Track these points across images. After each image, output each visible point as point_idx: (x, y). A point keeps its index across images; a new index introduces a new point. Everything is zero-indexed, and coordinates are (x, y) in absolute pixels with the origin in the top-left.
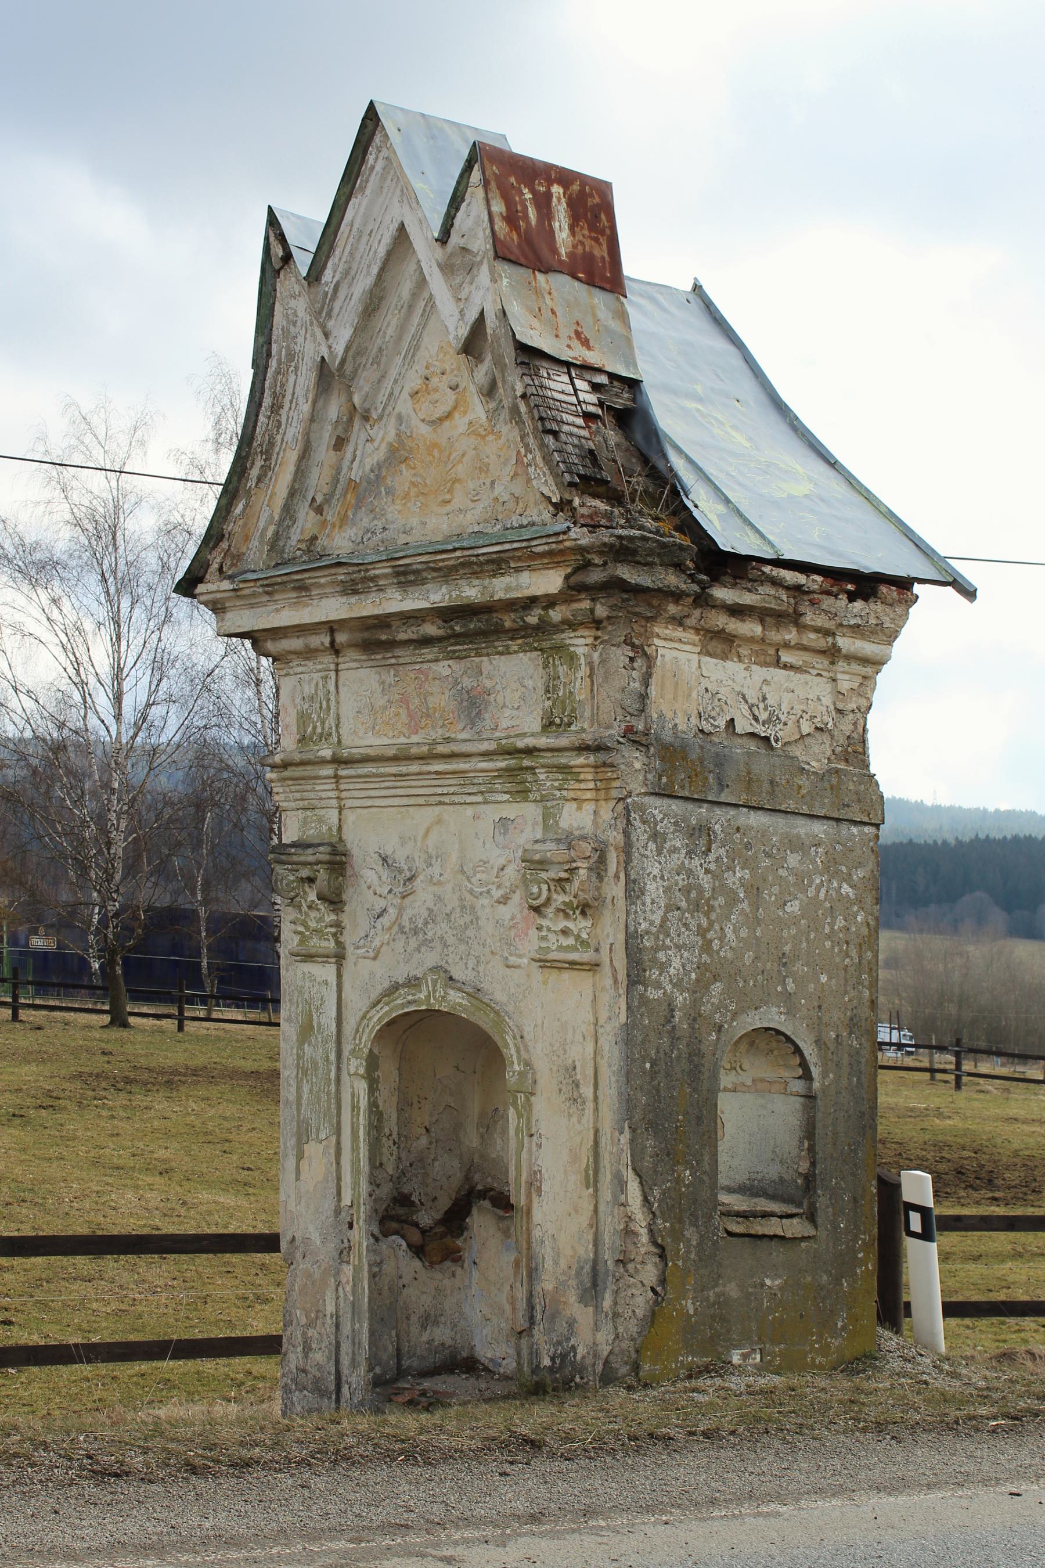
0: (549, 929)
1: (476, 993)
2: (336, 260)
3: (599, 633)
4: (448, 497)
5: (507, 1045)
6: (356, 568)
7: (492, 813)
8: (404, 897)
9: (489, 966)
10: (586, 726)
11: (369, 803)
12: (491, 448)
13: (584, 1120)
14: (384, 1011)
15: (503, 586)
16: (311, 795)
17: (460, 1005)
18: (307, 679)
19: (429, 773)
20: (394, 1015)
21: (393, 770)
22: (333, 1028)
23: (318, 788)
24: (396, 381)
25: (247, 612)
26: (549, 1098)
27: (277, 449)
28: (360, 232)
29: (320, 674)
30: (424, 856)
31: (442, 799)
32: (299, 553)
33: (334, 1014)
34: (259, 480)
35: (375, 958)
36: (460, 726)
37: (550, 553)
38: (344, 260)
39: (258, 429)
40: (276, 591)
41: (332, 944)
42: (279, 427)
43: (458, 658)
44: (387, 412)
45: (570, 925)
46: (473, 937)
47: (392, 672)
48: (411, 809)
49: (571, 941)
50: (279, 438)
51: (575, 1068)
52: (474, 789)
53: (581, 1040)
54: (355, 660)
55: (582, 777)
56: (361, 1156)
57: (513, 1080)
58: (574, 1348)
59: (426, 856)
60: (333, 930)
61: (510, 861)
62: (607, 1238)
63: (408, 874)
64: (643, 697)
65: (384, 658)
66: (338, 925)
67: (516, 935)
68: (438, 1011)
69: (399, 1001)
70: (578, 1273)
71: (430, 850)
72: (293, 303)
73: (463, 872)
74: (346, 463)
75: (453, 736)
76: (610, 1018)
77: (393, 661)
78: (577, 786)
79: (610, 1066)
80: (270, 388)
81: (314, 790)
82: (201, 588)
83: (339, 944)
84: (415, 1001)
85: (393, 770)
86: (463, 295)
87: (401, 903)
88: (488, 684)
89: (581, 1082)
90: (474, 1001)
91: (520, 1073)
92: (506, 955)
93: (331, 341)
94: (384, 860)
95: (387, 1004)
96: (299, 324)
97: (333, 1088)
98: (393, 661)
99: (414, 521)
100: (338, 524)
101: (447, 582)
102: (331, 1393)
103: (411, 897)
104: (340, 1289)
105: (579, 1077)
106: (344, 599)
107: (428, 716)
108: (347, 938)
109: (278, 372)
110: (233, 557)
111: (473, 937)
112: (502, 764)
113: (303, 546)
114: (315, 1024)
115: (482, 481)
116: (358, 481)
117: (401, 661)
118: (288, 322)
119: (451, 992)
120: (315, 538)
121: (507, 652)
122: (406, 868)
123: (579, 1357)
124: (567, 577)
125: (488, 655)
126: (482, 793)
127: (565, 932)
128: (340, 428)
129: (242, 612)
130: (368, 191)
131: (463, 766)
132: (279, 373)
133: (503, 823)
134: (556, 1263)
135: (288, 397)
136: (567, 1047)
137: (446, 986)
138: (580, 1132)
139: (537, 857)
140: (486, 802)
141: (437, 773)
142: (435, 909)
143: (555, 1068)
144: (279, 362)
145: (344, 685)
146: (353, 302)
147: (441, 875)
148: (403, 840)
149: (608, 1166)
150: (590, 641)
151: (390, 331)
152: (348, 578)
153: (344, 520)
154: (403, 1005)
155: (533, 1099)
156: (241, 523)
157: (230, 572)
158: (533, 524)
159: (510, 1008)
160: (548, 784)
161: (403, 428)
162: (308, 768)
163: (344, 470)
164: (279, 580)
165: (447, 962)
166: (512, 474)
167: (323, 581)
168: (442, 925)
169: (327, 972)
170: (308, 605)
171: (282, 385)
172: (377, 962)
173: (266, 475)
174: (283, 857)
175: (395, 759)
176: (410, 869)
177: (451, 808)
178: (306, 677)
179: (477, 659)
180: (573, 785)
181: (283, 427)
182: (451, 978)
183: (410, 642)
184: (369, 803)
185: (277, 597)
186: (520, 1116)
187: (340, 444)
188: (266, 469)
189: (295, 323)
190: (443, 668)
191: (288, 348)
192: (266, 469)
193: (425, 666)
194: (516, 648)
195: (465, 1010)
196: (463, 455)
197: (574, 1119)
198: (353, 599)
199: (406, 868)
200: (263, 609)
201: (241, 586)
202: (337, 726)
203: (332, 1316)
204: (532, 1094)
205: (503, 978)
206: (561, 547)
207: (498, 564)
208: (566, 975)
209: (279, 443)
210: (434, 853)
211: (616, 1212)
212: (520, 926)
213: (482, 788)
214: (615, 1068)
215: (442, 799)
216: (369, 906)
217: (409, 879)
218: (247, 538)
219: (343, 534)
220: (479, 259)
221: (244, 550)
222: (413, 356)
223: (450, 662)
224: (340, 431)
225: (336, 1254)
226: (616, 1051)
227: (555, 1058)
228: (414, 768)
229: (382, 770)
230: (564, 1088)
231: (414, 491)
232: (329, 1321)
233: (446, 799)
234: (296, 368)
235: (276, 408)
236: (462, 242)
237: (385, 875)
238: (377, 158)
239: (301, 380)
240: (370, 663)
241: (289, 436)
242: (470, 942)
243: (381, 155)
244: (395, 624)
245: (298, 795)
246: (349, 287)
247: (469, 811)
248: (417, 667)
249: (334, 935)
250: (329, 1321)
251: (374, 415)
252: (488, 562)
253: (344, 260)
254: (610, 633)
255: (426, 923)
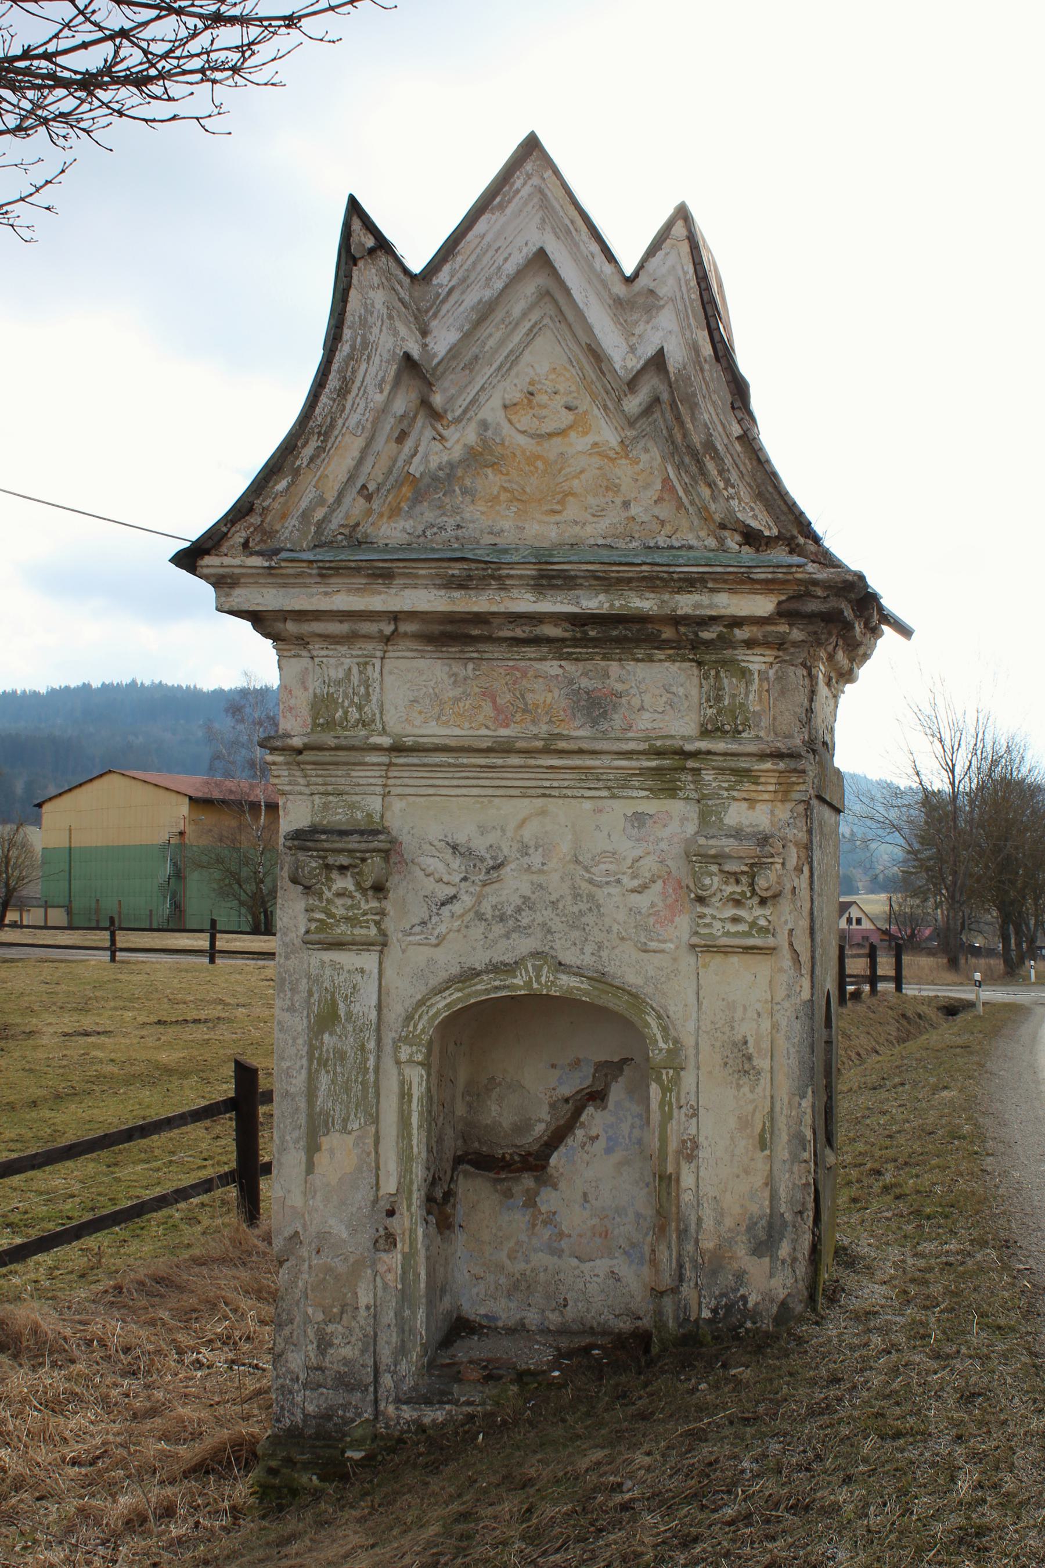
0: (714, 917)
1: (600, 979)
2: (457, 266)
3: (781, 653)
4: (558, 507)
5: (648, 1025)
6: (483, 566)
7: (619, 809)
9: (617, 951)
10: (762, 734)
12: (624, 472)
13: (759, 1090)
15: (690, 603)
16: (342, 781)
17: (578, 989)
18: (338, 664)
19: (539, 767)
21: (482, 761)
22: (373, 1015)
23: (354, 774)
24: (482, 388)
25: (273, 591)
26: (710, 1072)
27: (336, 433)
28: (489, 246)
29: (356, 660)
30: (516, 846)
31: (547, 792)
32: (340, 537)
33: (374, 1001)
34: (312, 460)
36: (577, 723)
37: (767, 581)
38: (465, 267)
39: (318, 410)
40: (330, 576)
41: (373, 931)
42: (343, 411)
43: (577, 660)
44: (468, 416)
45: (742, 913)
46: (592, 923)
47: (470, 666)
49: (743, 927)
50: (340, 422)
51: (746, 1043)
52: (600, 784)
53: (755, 1016)
54: (412, 650)
55: (762, 780)
56: (415, 1142)
57: (659, 1057)
58: (744, 1298)
60: (377, 918)
62: (783, 1194)
63: (491, 863)
64: (810, 711)
65: (461, 652)
66: (382, 913)
67: (657, 922)
69: (479, 987)
70: (750, 1229)
72: (372, 294)
73: (577, 862)
74: (403, 457)
75: (565, 732)
76: (789, 996)
77: (475, 655)
78: (753, 787)
79: (788, 1038)
80: (339, 372)
81: (348, 775)
82: (207, 560)
83: (383, 933)
84: (505, 987)
85: (482, 761)
86: (637, 331)
88: (619, 687)
89: (755, 1055)
90: (597, 985)
91: (669, 1051)
92: (643, 940)
93: (428, 340)
94: (455, 848)
95: (459, 990)
96: (375, 314)
97: (371, 1077)
98: (475, 655)
99: (506, 525)
100: (386, 514)
101: (606, 592)
102: (366, 1387)
103: (496, 886)
104: (378, 1279)
105: (751, 1051)
106: (442, 592)
107: (525, 711)
108: (388, 924)
109: (350, 357)
110: (264, 533)
111: (592, 923)
112: (653, 764)
113: (346, 531)
114: (342, 1013)
115: (608, 499)
116: (418, 475)
117: (486, 656)
118: (366, 310)
119: (564, 977)
120: (358, 525)
121: (650, 659)
122: (488, 856)
123: (750, 1305)
124: (780, 603)
125: (620, 660)
126: (609, 788)
127: (735, 920)
128: (406, 422)
129: (265, 591)
130: (508, 211)
131: (589, 762)
132: (352, 359)
133: (639, 819)
134: (719, 1223)
135: (357, 384)
136: (736, 1025)
137: (557, 971)
138: (754, 1100)
139: (713, 852)
141: (552, 767)
142: (533, 897)
143: (718, 1044)
144: (353, 347)
145: (391, 673)
146: (462, 309)
147: (543, 864)
148: (483, 830)
149: (784, 1128)
150: (770, 659)
151: (491, 343)
152: (465, 573)
153: (395, 512)
154: (487, 991)
155: (682, 1073)
156: (282, 500)
157: (257, 548)
158: (691, 548)
159: (649, 990)
160: (714, 784)
161: (489, 433)
162: (353, 753)
163: (400, 463)
164: (353, 565)
165: (552, 948)
166: (655, 498)
167: (422, 572)
168: (544, 912)
169: (369, 961)
170: (380, 593)
171: (354, 372)
173: (318, 456)
174: (309, 844)
175: (489, 750)
176: (493, 858)
177: (560, 801)
178: (332, 661)
179: (603, 663)
180: (747, 786)
181: (347, 411)
182: (560, 964)
183: (506, 639)
184: (431, 791)
185: (332, 580)
186: (665, 1090)
187: (402, 437)
188: (320, 450)
189: (372, 313)
190: (552, 667)
191: (364, 336)
192: (320, 450)
193: (522, 664)
194: (663, 657)
195: (586, 993)
196: (582, 472)
197: (746, 1089)
198: (457, 594)
199: (488, 856)
200: (303, 590)
201: (283, 564)
202: (381, 713)
203: (368, 1308)
204: (682, 1069)
206: (790, 577)
207: (690, 583)
208: (735, 959)
209: (339, 427)
210: (532, 843)
211: (796, 1168)
214: (796, 1040)
215: (565, 791)
217: (493, 868)
218: (284, 517)
219: (393, 525)
220: (662, 303)
221: (278, 527)
222: (510, 369)
223: (563, 663)
224: (404, 425)
225: (370, 1245)
226: (797, 1026)
227: (719, 1034)
228: (515, 760)
229: (465, 761)
230: (731, 1062)
231: (504, 496)
232: (363, 1312)
233: (569, 792)
234: (369, 357)
235: (343, 392)
236: (652, 285)
237: (456, 863)
238: (525, 184)
239: (372, 370)
240: (441, 655)
241: (352, 421)
243: (530, 182)
244: (496, 622)
245: (320, 780)
246: (463, 293)
247: (588, 805)
248: (511, 663)
249: (377, 923)
250: (363, 1312)
251: (450, 417)
252: (680, 579)
253: (465, 267)
254: (792, 654)
255: (519, 910)
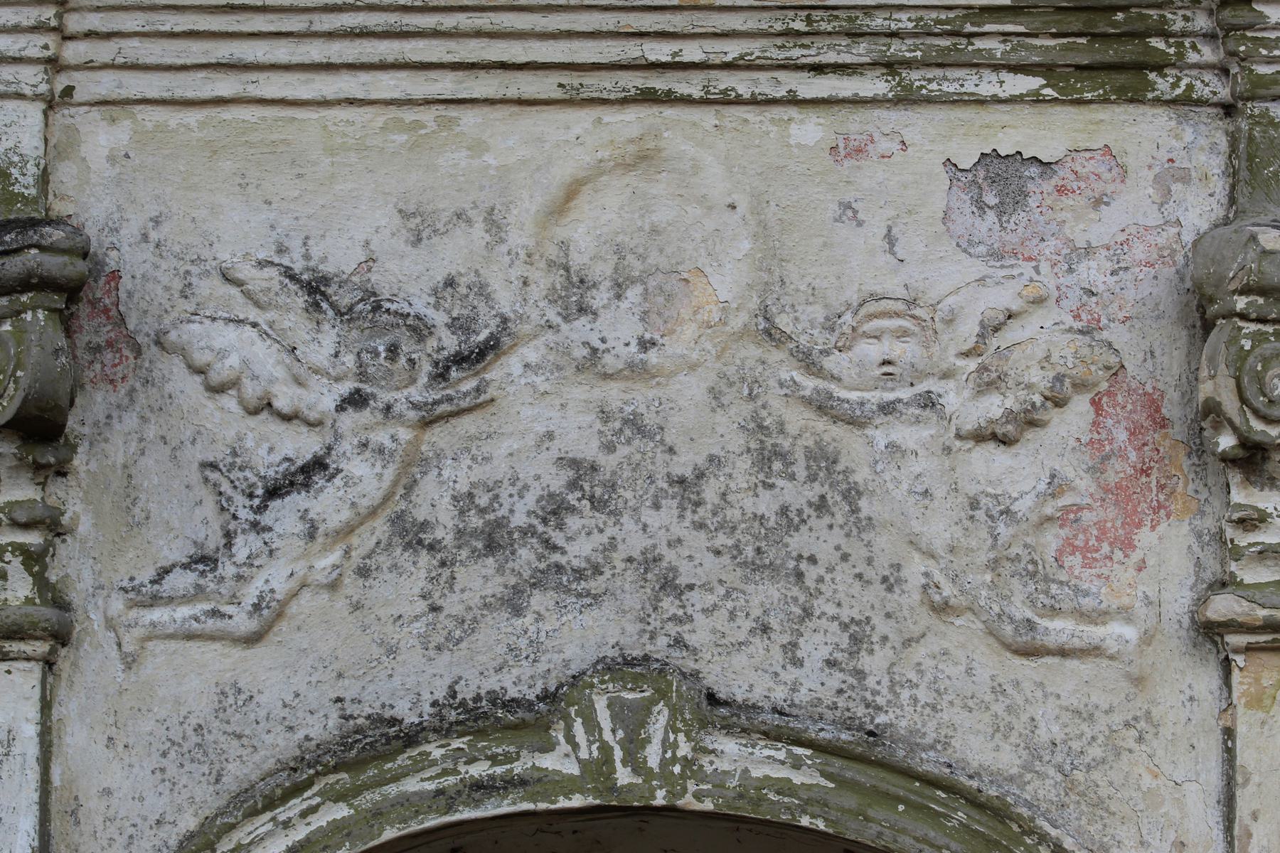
7: (935, 141)
8: (426, 424)
11: (226, 86)
14: (320, 821)
17: (784, 787)
20: (390, 834)
31: (659, 83)
35: (252, 640)
48: (469, 118)
52: (861, 52)
59: (558, 278)
61: (1039, 301)
63: (451, 343)
66: (52, 525)
68: (670, 811)
69: (412, 785)
71: (576, 260)
83: (52, 595)
87: (415, 443)
90: (853, 772)
103: (467, 424)
108: (74, 566)
133: (1002, 178)
140: (906, 99)
148: (419, 227)
159: (1042, 789)
172: (259, 651)
177: (707, 117)
182: (712, 699)
184: (226, 86)
205: (998, 690)
212: (1087, 516)
213: (897, 49)
216: (218, 453)
242: (811, 573)
247: (810, 130)
